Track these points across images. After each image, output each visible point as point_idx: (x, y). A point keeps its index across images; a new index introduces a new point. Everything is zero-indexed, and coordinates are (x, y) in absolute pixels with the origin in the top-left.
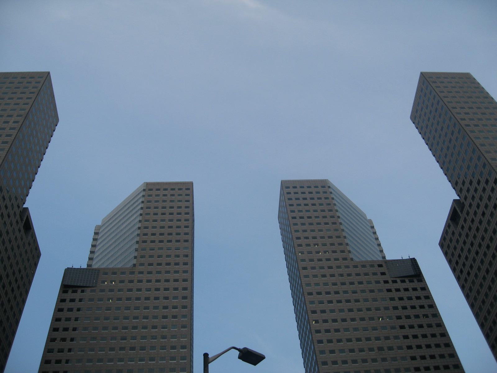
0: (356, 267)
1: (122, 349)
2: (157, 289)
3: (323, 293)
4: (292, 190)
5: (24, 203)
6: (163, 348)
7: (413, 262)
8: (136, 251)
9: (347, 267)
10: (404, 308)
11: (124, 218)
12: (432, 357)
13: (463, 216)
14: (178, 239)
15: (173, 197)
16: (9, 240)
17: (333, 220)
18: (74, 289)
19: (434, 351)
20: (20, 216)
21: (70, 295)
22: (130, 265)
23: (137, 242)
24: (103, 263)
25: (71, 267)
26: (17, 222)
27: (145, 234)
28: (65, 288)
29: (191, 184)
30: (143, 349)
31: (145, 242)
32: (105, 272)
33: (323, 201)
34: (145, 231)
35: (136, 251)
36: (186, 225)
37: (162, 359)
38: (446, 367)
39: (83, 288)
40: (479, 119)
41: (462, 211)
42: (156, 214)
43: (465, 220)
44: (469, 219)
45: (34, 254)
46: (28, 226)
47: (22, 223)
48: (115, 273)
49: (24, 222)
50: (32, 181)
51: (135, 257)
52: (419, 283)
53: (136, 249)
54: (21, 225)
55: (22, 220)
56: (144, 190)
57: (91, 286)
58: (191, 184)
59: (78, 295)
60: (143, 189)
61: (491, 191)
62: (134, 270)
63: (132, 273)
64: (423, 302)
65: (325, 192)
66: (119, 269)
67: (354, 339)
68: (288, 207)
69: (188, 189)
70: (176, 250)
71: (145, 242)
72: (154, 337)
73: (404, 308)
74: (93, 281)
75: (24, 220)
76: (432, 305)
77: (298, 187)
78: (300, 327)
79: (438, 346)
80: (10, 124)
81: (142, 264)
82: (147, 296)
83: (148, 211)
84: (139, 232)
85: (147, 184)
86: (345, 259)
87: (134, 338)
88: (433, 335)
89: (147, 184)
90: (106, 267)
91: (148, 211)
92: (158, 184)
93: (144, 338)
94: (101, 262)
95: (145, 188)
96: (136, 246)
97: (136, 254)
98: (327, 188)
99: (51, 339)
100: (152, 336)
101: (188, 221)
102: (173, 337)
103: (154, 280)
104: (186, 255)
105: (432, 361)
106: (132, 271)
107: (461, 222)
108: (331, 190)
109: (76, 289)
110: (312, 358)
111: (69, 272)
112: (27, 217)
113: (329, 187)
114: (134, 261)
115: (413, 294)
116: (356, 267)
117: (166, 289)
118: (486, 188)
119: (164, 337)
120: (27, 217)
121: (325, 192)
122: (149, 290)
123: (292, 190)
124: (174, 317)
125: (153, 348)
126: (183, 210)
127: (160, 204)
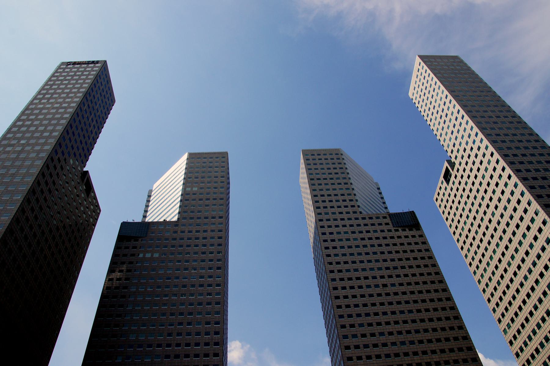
0: (364, 218)
2: (197, 238)
3: (342, 263)
4: (311, 157)
7: (412, 214)
9: (357, 219)
10: (405, 252)
12: (443, 329)
13: (453, 173)
15: (211, 164)
17: (345, 181)
19: (442, 314)
28: (120, 238)
29: (227, 153)
33: (337, 166)
38: (465, 361)
39: (136, 239)
40: (495, 123)
41: (453, 170)
43: (456, 177)
44: (459, 176)
52: (418, 232)
59: (133, 243)
64: (428, 262)
65: (338, 159)
67: (375, 324)
68: (324, 251)
69: (223, 157)
73: (405, 252)
76: (466, 336)
77: (316, 154)
78: (318, 269)
79: (444, 309)
86: (355, 212)
88: (440, 300)
98: (340, 155)
105: (443, 333)
107: (452, 178)
108: (343, 157)
110: (331, 312)
111: (125, 226)
113: (342, 154)
115: (439, 305)
116: (364, 218)
117: (205, 238)
118: (499, 183)
121: (338, 159)
123: (311, 157)
126: (216, 241)
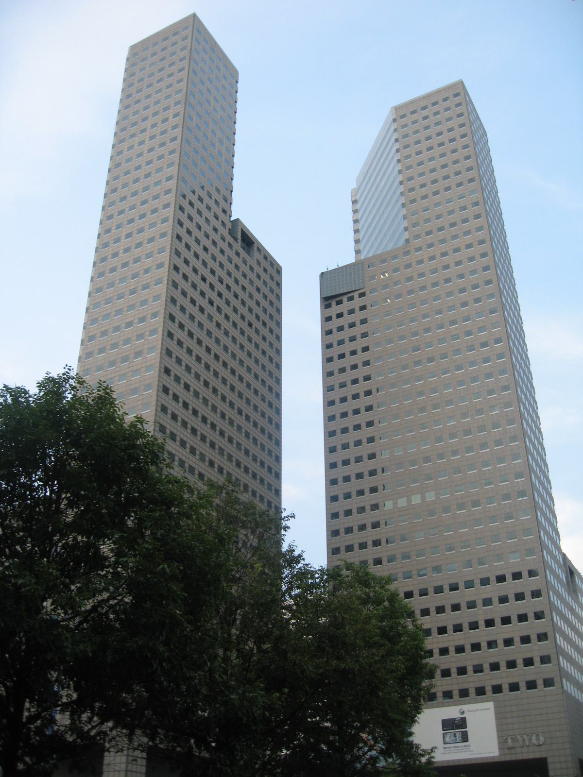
1: (417, 363)
5: (230, 216)
6: (471, 348)
8: (404, 219)
11: (376, 178)
14: (459, 181)
16: (243, 262)
18: (338, 299)
20: (232, 236)
21: (335, 309)
22: (401, 243)
23: (404, 205)
24: (377, 248)
25: (337, 267)
26: (230, 245)
27: (412, 190)
28: (327, 301)
29: (461, 83)
30: (444, 356)
31: (413, 201)
32: (382, 258)
34: (411, 184)
35: (404, 219)
36: (467, 155)
37: (473, 363)
42: (419, 153)
45: (272, 272)
46: (248, 241)
47: (237, 242)
48: (384, 261)
49: (240, 241)
50: (230, 180)
51: (406, 229)
53: (405, 217)
54: (238, 246)
55: (236, 239)
56: (394, 120)
57: (357, 288)
58: (461, 83)
60: (392, 119)
61: (122, 264)
62: (408, 249)
63: (407, 253)
66: (374, 257)
70: (459, 199)
71: (413, 201)
72: (456, 337)
74: (359, 281)
75: (239, 237)
80: (170, 120)
81: (417, 237)
82: (435, 281)
83: (407, 151)
84: (402, 189)
85: (397, 109)
87: (429, 344)
89: (396, 110)
90: (394, 247)
91: (407, 151)
92: (412, 102)
93: (441, 341)
94: (375, 248)
95: (395, 117)
96: (404, 211)
97: (405, 224)
99: (328, 373)
100: (452, 336)
101: (468, 147)
102: (481, 329)
103: (438, 256)
104: (475, 203)
106: (405, 250)
109: (340, 298)
112: (242, 231)
114: (406, 235)
119: (469, 333)
120: (242, 231)
122: (434, 271)
124: (477, 300)
125: (457, 351)
127: (422, 135)
